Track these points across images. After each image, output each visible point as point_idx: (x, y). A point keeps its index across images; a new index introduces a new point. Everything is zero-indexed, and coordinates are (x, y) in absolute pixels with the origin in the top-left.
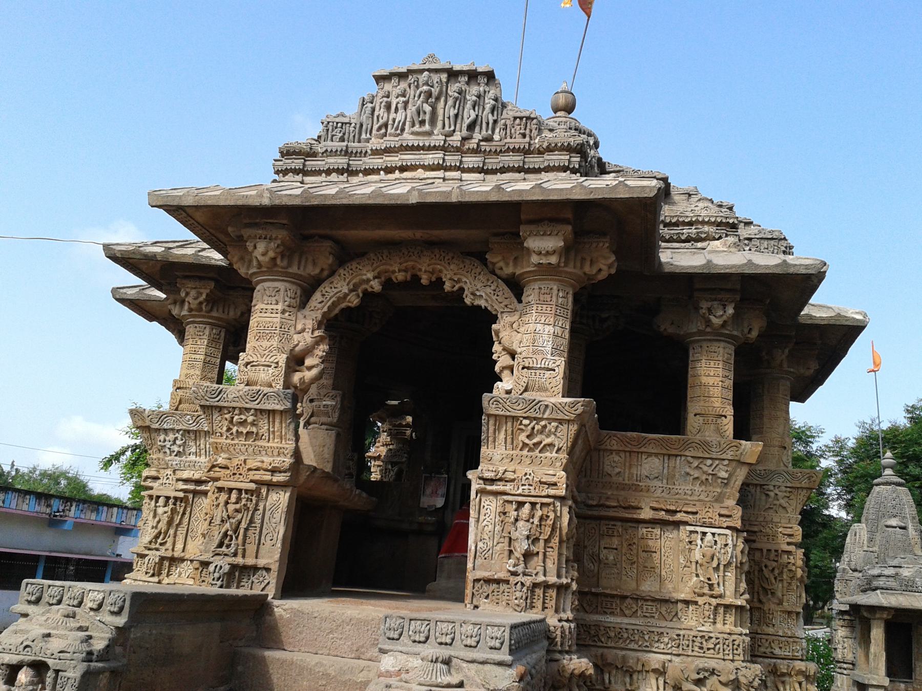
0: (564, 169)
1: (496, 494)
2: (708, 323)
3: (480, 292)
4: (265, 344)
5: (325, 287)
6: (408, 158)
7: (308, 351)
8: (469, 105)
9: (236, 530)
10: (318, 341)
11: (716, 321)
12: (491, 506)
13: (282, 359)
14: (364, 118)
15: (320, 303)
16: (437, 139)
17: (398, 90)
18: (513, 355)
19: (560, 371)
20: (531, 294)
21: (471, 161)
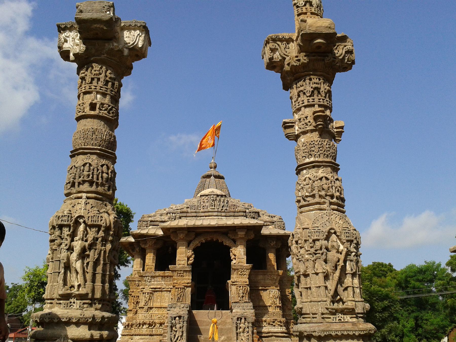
0: (243, 216)
1: (235, 285)
2: (270, 245)
3: (227, 243)
4: (182, 255)
5: (193, 242)
6: (210, 214)
7: (191, 257)
8: (222, 202)
9: (181, 296)
10: (192, 254)
11: (272, 245)
12: (234, 288)
13: (186, 259)
14: (199, 204)
15: (193, 245)
16: (216, 210)
17: (206, 198)
18: (235, 256)
19: (245, 258)
20: (238, 243)
21: (223, 214)
